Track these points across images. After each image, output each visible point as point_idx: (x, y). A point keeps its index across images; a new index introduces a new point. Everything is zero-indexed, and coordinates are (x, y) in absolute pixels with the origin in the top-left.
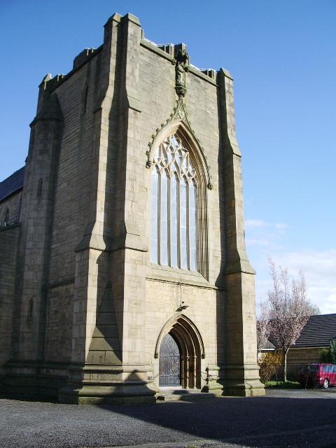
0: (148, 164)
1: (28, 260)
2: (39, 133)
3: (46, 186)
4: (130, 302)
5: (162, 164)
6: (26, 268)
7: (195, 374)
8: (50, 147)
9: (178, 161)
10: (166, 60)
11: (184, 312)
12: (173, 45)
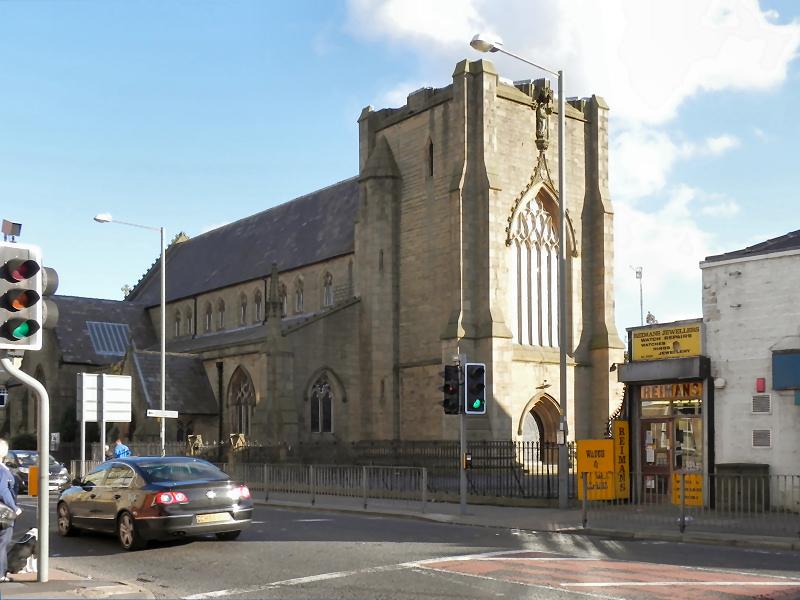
0: (508, 242)
1: (375, 339)
2: (373, 194)
3: (388, 257)
4: (498, 385)
5: (521, 237)
6: (374, 347)
8: (389, 211)
9: (539, 231)
11: (547, 390)
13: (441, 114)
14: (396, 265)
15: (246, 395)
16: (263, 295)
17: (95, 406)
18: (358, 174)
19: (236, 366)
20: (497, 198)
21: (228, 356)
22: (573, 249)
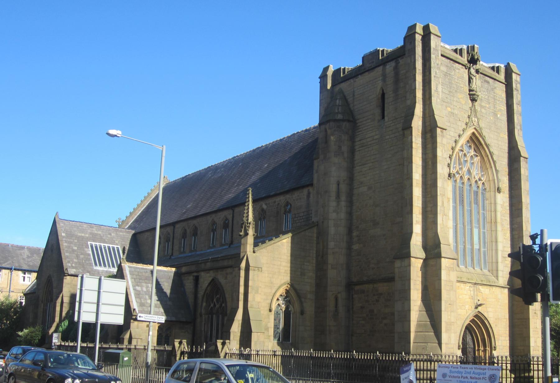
3: (344, 187)
6: (330, 266)
7: (75, 376)
8: (345, 149)
10: (461, 66)
11: (480, 309)
12: (465, 47)
13: (392, 68)
14: (350, 194)
15: (217, 306)
16: (231, 222)
17: (425, 365)
18: (316, 123)
19: (210, 279)
20: (443, 136)
21: (204, 270)
22: (119, 262)
